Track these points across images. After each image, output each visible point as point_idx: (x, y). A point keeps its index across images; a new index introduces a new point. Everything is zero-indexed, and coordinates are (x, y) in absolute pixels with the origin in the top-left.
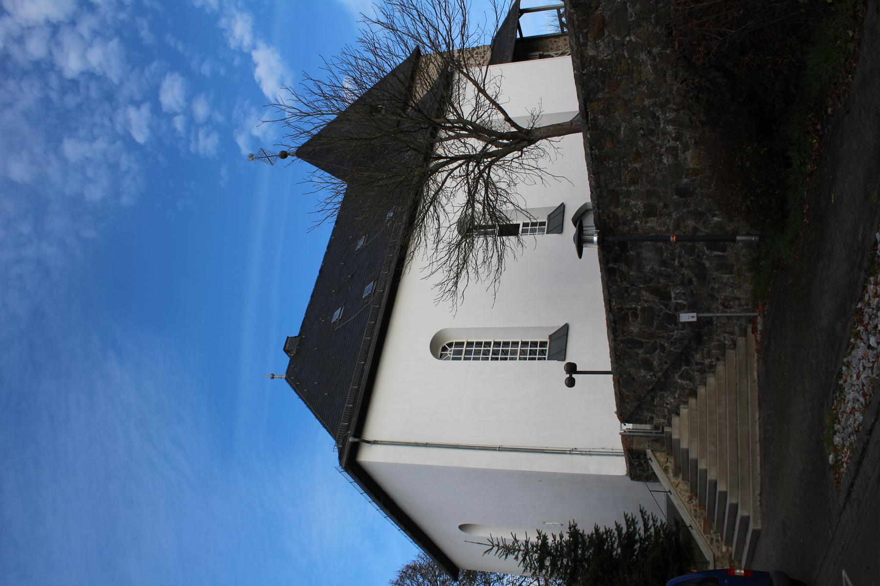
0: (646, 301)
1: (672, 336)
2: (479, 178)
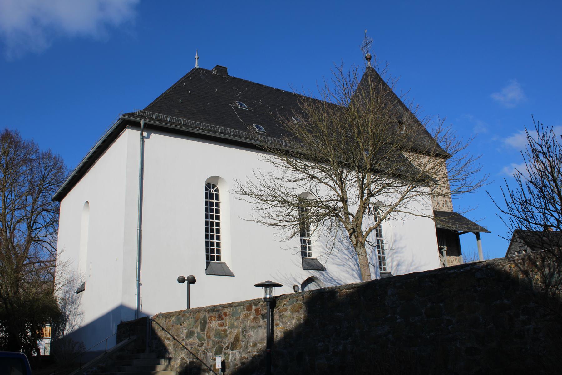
0: (230, 333)
1: (208, 352)
2: (552, 171)
